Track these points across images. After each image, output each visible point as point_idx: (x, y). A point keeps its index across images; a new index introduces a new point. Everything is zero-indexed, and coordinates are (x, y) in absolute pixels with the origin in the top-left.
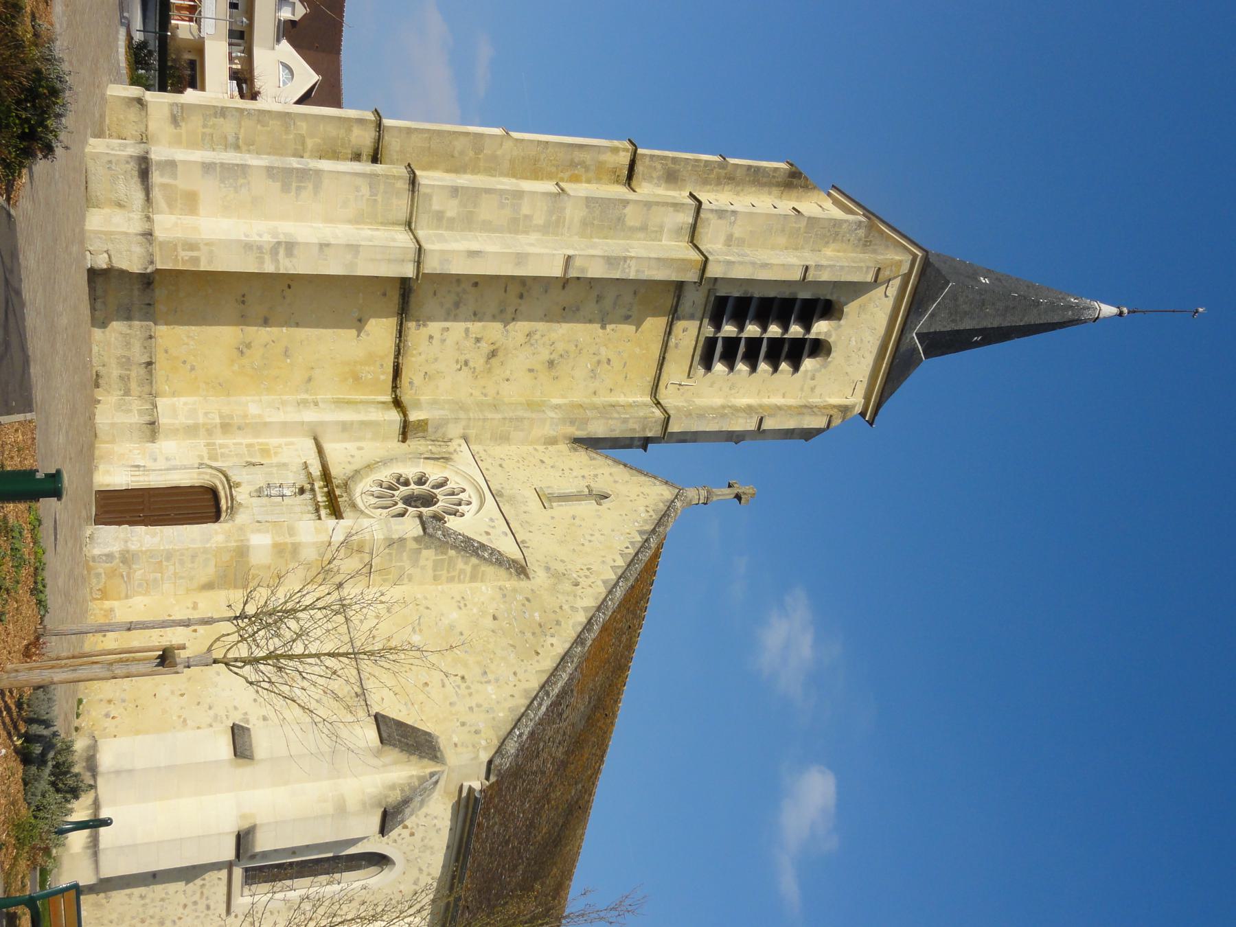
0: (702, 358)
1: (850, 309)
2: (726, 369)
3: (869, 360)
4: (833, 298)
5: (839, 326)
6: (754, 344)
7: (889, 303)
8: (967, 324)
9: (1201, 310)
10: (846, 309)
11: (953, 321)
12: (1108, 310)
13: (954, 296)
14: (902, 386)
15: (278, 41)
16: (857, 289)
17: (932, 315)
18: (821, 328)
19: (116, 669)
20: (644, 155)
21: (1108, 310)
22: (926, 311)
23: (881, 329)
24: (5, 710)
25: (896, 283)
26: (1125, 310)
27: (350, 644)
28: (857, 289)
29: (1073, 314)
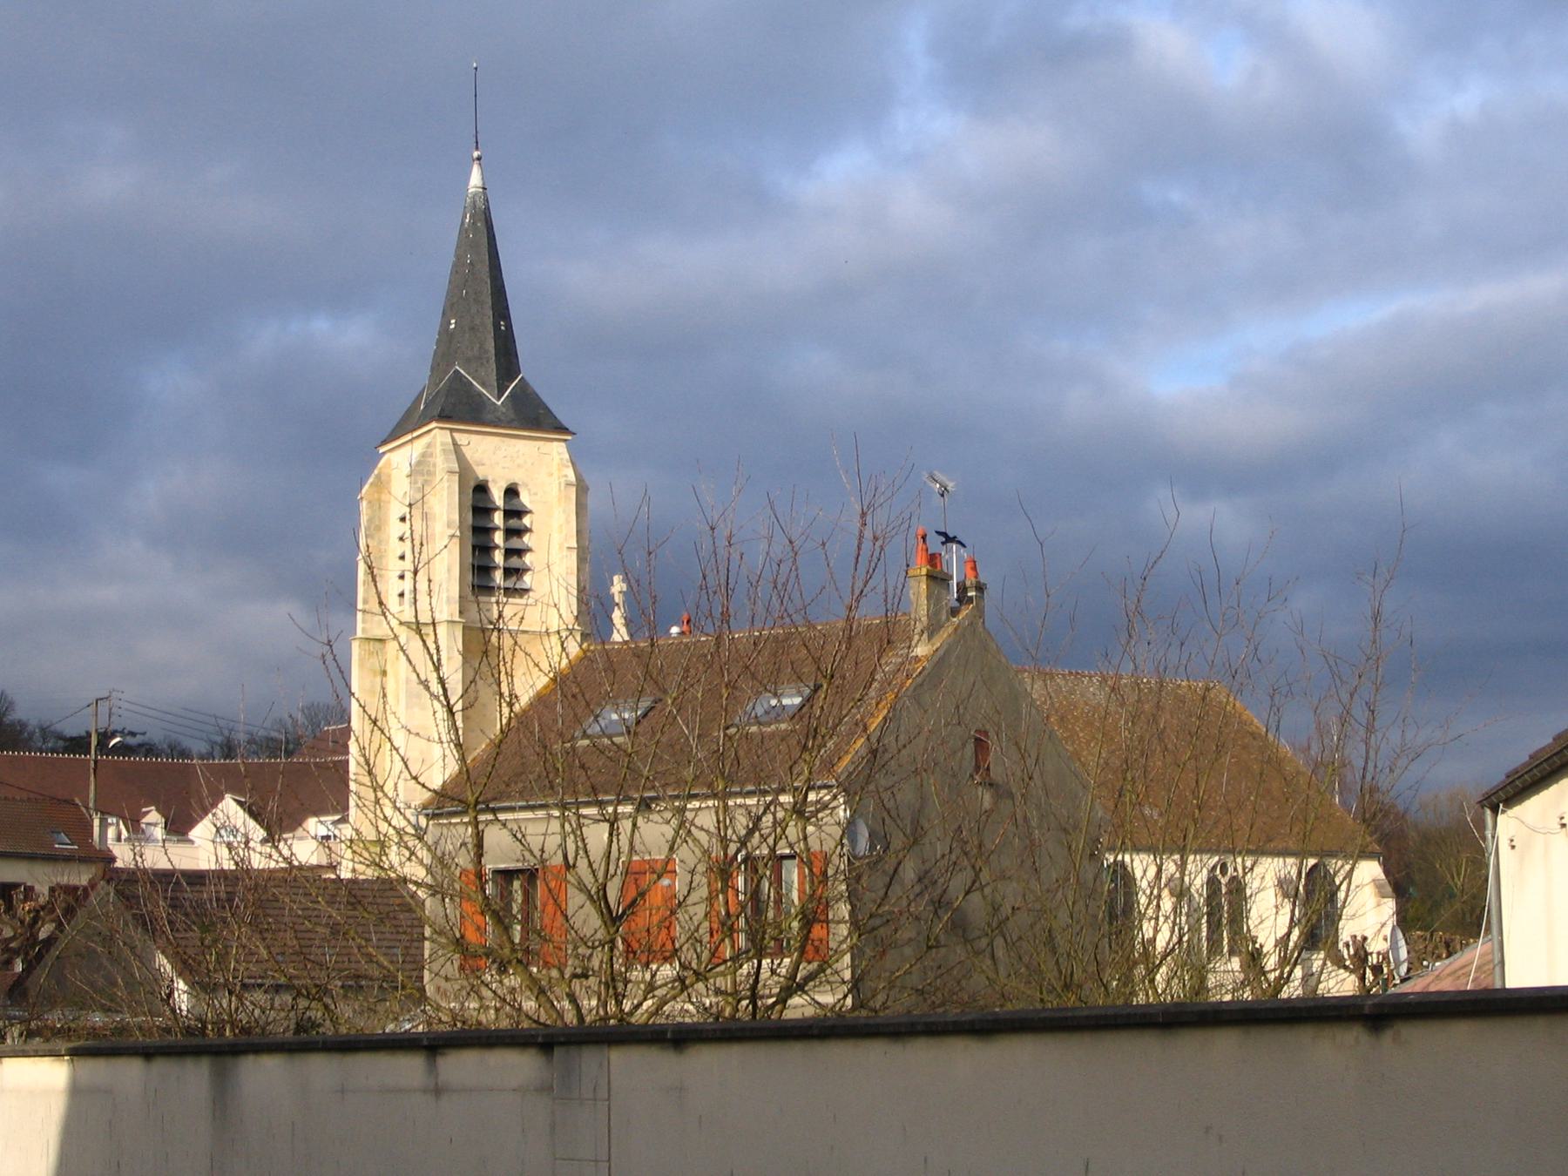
0: (521, 597)
1: (481, 473)
2: (530, 573)
3: (521, 444)
4: (472, 484)
5: (493, 481)
6: (509, 553)
7: (474, 438)
8: (490, 345)
9: (475, 65)
10: (481, 478)
11: (488, 362)
12: (475, 179)
13: (466, 363)
14: (538, 391)
15: (192, 842)
16: (464, 469)
17: (483, 385)
18: (498, 497)
19: (541, 919)
20: (364, 630)
21: (475, 179)
22: (480, 395)
23: (496, 440)
24: (96, 811)
25: (456, 435)
26: (476, 154)
27: (911, 573)
28: (464, 469)
29: (480, 220)
